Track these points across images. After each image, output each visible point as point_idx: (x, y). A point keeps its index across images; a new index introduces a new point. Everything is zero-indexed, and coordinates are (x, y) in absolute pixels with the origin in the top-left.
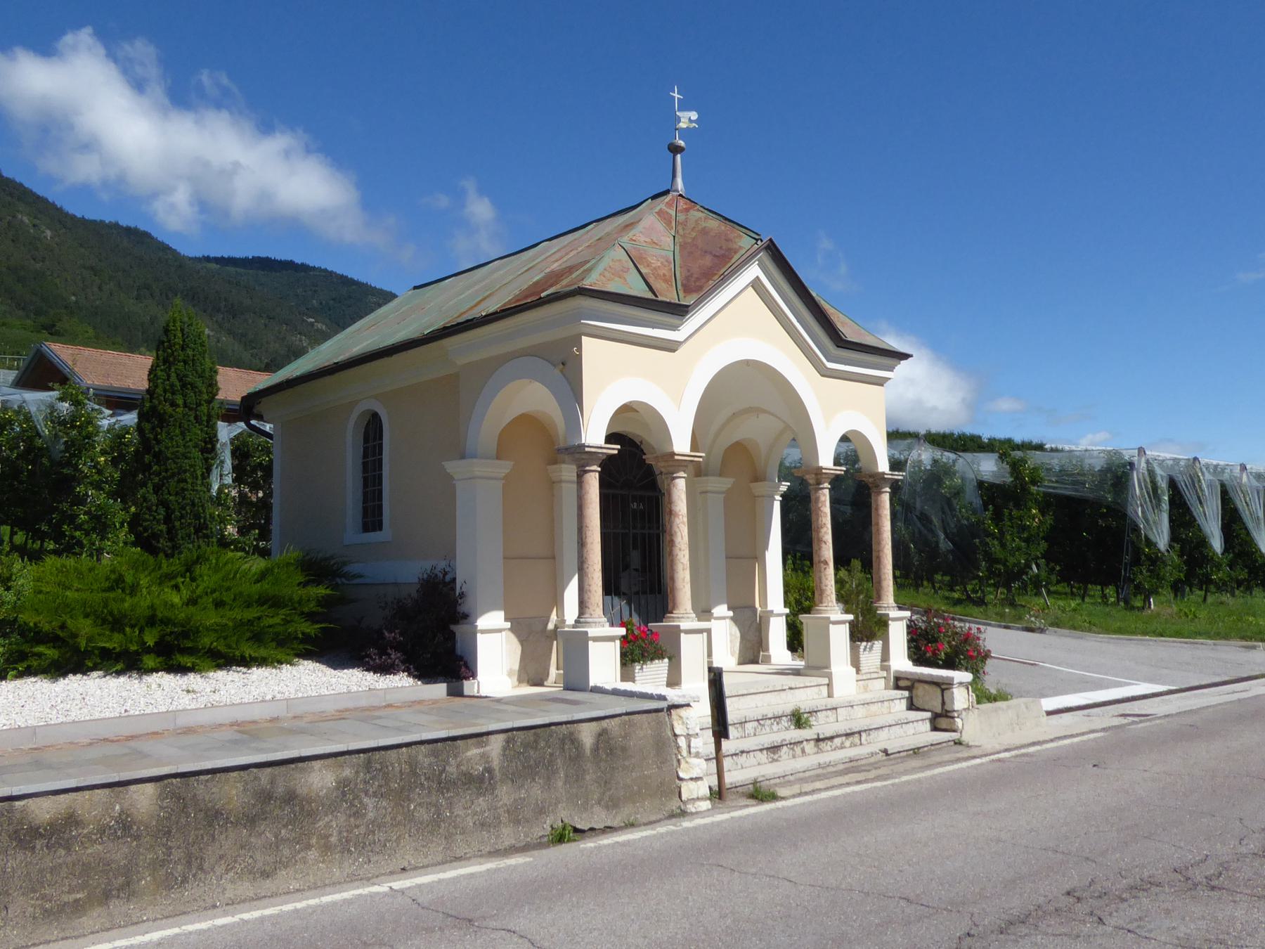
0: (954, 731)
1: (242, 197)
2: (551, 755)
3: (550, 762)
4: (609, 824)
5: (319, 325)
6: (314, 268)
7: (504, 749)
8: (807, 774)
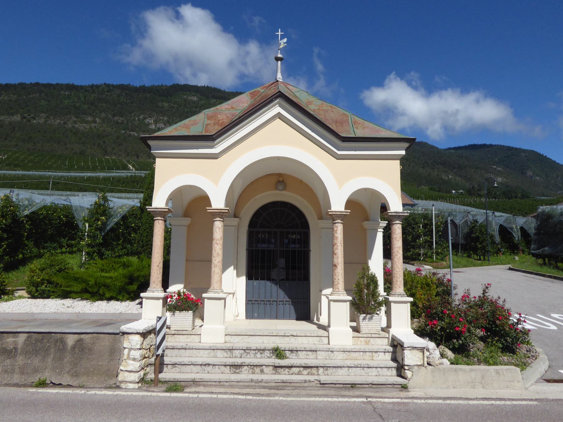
0: (406, 379)
1: (460, 123)
2: (49, 346)
3: (47, 350)
4: (70, 384)
5: (499, 169)
6: (495, 145)
7: (25, 340)
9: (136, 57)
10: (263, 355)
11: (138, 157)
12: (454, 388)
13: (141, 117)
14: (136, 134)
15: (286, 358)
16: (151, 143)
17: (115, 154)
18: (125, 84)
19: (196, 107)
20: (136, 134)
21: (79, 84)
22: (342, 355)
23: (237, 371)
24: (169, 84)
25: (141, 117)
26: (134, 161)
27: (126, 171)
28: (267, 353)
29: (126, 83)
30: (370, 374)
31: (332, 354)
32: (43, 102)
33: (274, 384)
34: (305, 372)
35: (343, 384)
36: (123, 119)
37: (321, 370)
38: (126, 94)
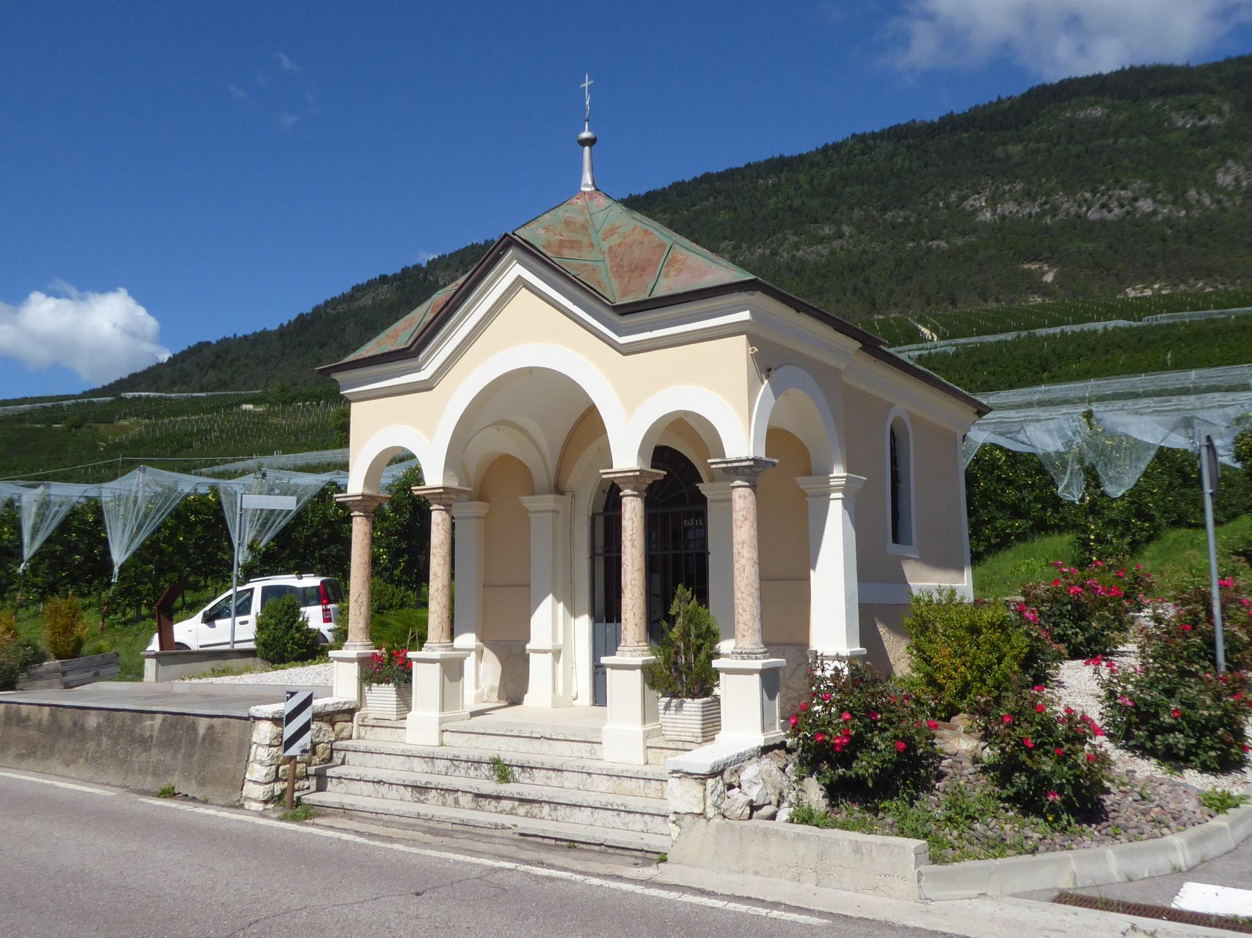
8: (404, 820)
9: (923, 48)
10: (479, 773)
11: (954, 303)
12: (756, 873)
13: (953, 197)
14: (943, 244)
15: (516, 781)
16: (338, 376)
17: (896, 305)
18: (903, 122)
19: (1103, 135)
20: (943, 244)
21: (795, 153)
22: (607, 784)
23: (422, 798)
24: (1018, 91)
25: (953, 197)
26: (935, 316)
27: (915, 346)
28: (485, 769)
29: (903, 120)
30: (631, 826)
31: (589, 780)
32: (723, 215)
33: (449, 827)
34: (522, 810)
35: (556, 839)
36: (908, 213)
37: (546, 808)
38: (909, 147)
